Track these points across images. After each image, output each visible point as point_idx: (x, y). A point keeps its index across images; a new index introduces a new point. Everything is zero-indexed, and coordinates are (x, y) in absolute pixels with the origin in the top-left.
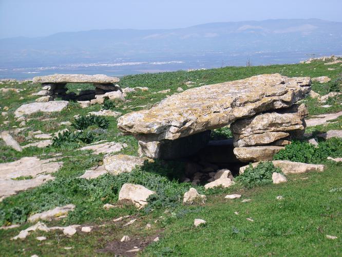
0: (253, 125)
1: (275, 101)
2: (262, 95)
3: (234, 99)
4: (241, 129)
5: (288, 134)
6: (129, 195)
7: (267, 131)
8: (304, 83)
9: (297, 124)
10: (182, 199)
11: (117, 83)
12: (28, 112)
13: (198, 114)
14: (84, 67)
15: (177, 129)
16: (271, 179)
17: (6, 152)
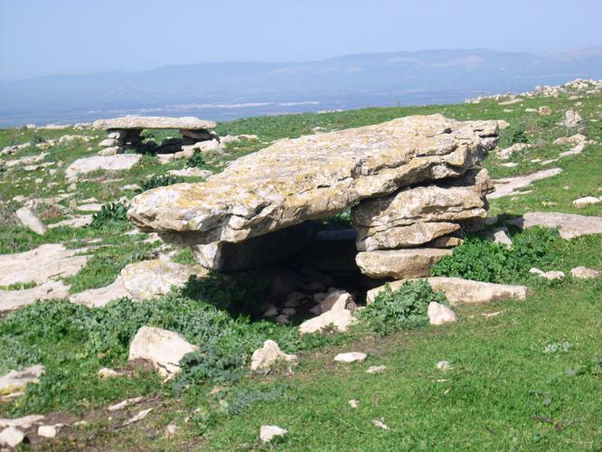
0: (394, 211)
1: (433, 164)
3: (358, 161)
4: (370, 218)
5: (458, 226)
6: (148, 351)
7: (419, 220)
8: (486, 132)
9: (474, 208)
10: (249, 361)
11: (213, 129)
12: (84, 171)
13: (288, 190)
14: (197, 108)
15: (243, 221)
16: (426, 315)
17: (19, 236)
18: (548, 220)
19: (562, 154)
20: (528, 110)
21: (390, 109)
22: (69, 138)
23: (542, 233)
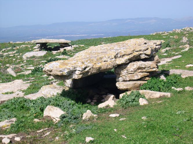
0: (128, 69)
1: (141, 54)
2: (133, 51)
4: (121, 71)
5: (148, 74)
8: (158, 44)
9: (154, 68)
10: (82, 117)
11: (70, 43)
12: (29, 56)
14: (64, 37)
15: (80, 72)
17: (8, 77)
18: (177, 72)
19: (182, 51)
20: (171, 37)
21: (126, 37)
22: (24, 46)
23: (175, 76)
